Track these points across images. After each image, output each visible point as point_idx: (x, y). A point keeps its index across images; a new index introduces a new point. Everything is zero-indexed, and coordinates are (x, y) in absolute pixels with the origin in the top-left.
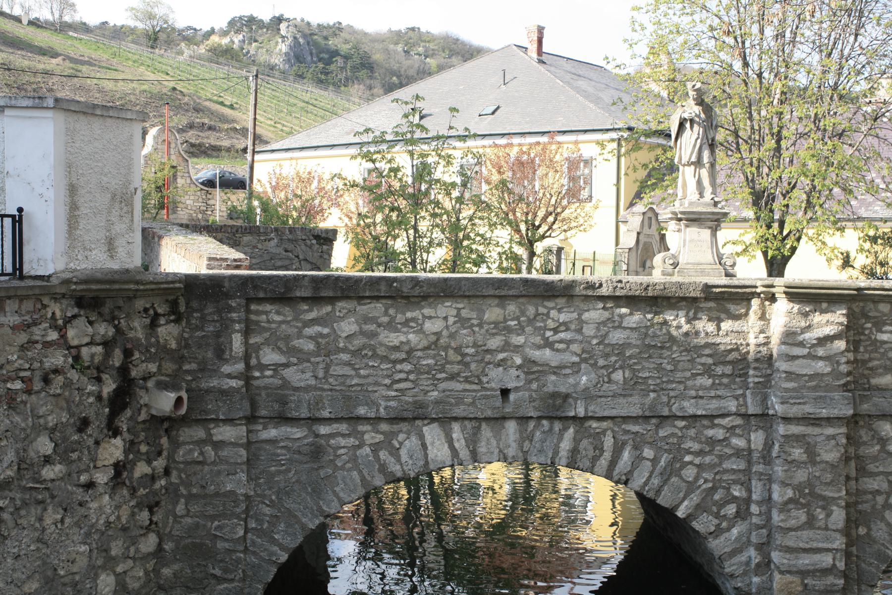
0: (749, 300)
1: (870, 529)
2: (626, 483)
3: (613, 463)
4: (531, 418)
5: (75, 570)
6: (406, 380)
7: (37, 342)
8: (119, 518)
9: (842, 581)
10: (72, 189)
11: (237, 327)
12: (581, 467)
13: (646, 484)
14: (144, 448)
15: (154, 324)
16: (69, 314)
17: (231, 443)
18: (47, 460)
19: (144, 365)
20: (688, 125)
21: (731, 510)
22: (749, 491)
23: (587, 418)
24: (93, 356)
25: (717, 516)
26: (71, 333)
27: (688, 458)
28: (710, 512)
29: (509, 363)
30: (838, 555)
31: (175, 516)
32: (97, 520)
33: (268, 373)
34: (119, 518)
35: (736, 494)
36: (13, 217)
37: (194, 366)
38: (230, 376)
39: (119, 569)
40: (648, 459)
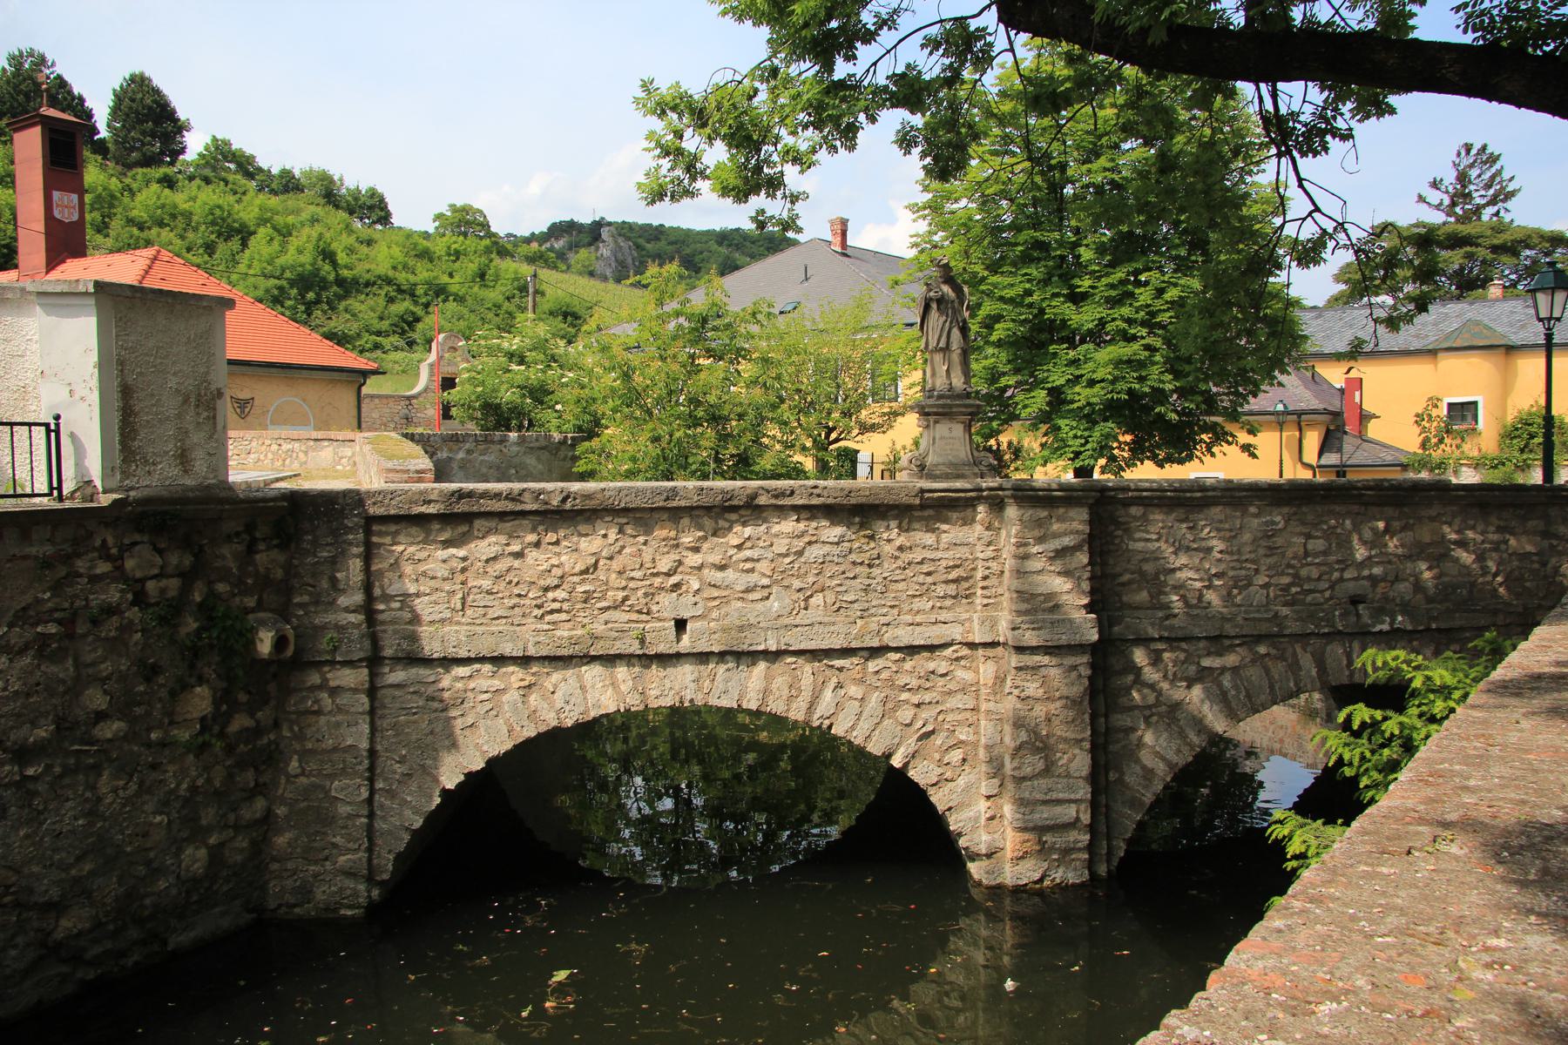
0: (974, 507)
1: (1122, 774)
5: (148, 845)
6: (559, 611)
7: (81, 576)
8: (209, 781)
9: (1088, 837)
10: (126, 392)
11: (355, 550)
13: (853, 728)
14: (243, 697)
15: (251, 550)
16: (127, 541)
17: (350, 689)
18: (100, 716)
19: (237, 599)
20: (934, 306)
21: (956, 756)
24: (163, 591)
26: (129, 564)
29: (684, 588)
30: (1083, 807)
31: (288, 776)
32: (178, 785)
33: (397, 605)
34: (209, 781)
36: (47, 425)
37: (306, 598)
38: (347, 610)
39: (212, 841)
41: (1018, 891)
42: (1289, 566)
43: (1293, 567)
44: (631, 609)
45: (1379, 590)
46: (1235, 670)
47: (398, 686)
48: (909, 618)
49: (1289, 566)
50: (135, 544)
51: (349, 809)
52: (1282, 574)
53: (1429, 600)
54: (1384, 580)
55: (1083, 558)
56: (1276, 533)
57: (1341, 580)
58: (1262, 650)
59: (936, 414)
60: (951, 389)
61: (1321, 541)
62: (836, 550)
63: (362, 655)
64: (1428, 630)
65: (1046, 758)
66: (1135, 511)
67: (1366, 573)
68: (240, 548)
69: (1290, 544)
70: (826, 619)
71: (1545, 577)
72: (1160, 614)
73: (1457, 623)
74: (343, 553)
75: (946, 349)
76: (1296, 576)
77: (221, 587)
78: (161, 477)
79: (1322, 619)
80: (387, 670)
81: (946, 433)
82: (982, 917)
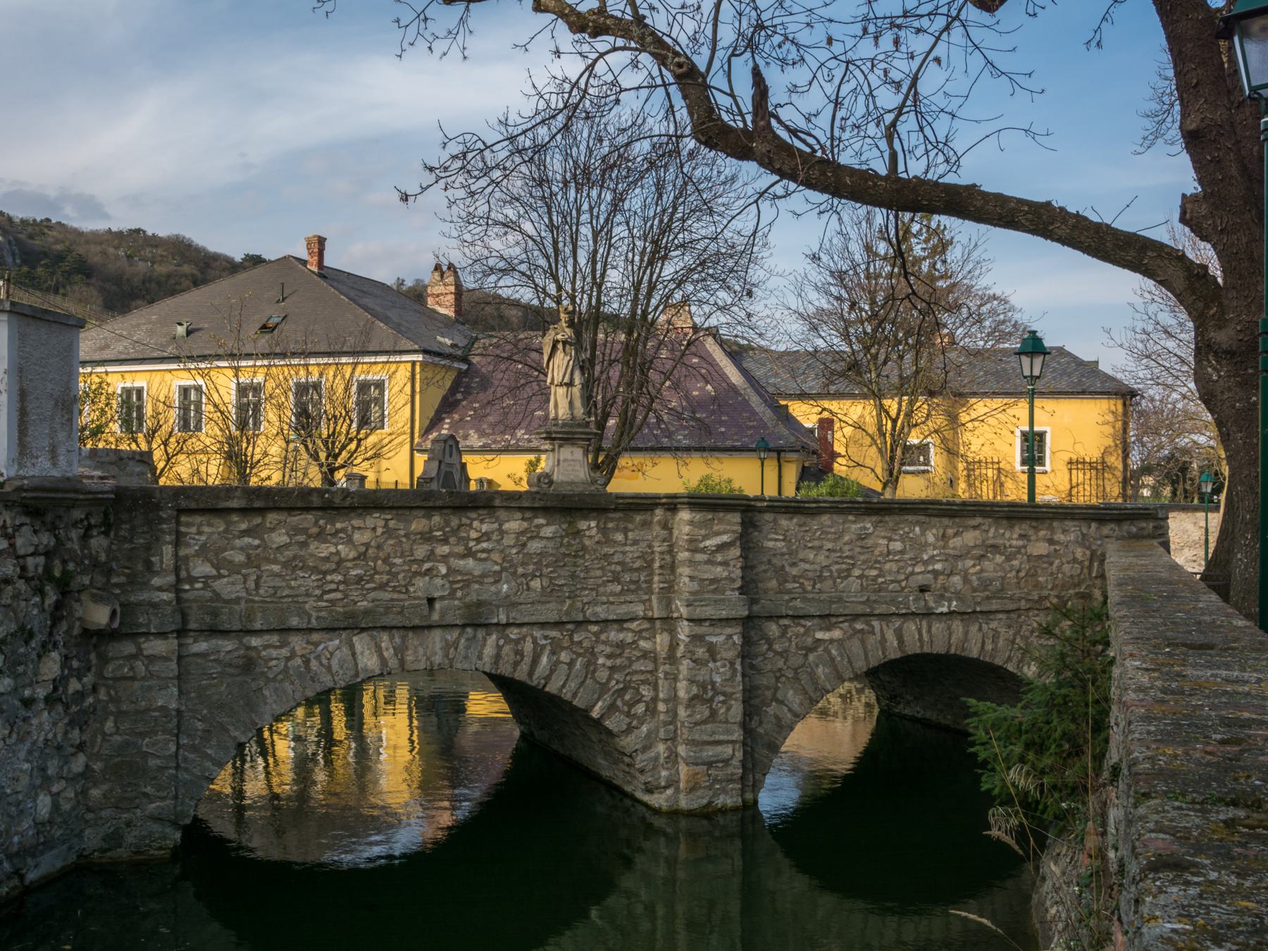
10: (23, 395)
11: (168, 538)
13: (563, 686)
16: (17, 523)
20: (560, 346)
26: (19, 542)
31: (104, 734)
33: (198, 585)
37: (123, 579)
38: (160, 589)
41: (690, 814)
42: (876, 562)
43: (879, 562)
44: (394, 589)
45: (940, 581)
46: (840, 642)
47: (202, 655)
49: (876, 562)
50: (22, 525)
51: (158, 762)
52: (871, 568)
53: (975, 590)
54: (942, 573)
55: (736, 552)
56: (868, 536)
57: (912, 573)
58: (859, 626)
59: (560, 439)
60: (573, 418)
61: (898, 543)
62: (550, 544)
63: (173, 627)
64: (974, 612)
66: (768, 517)
67: (930, 568)
69: (877, 545)
70: (543, 599)
71: (1052, 574)
72: (787, 597)
73: (994, 607)
74: (157, 539)
75: (570, 384)
76: (880, 570)
77: (71, 566)
78: (41, 468)
79: (900, 603)
80: (190, 641)
81: (569, 457)
82: (662, 839)
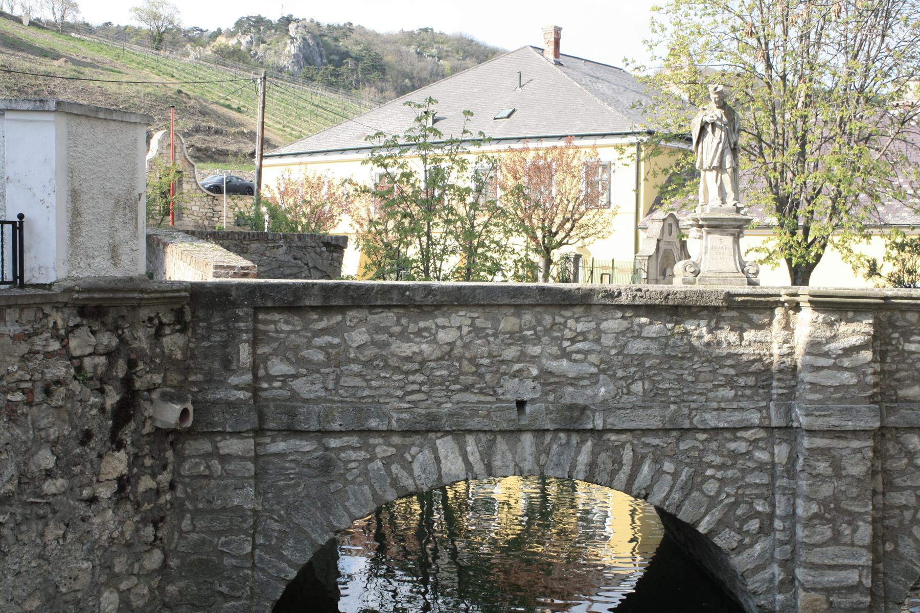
0: (773, 309)
1: (897, 545)
2: (645, 498)
3: (632, 477)
4: (548, 430)
5: (77, 588)
6: (419, 391)
7: (38, 352)
8: (122, 533)
9: (869, 599)
10: (75, 195)
11: (245, 336)
12: (599, 481)
13: (666, 498)
14: (148, 462)
15: (158, 334)
16: (71, 324)
17: (239, 456)
18: (49, 474)
20: (709, 129)
21: (754, 525)
22: (773, 506)
23: (605, 431)
24: (95, 367)
25: (739, 531)
26: (73, 343)
27: (709, 472)
28: (732, 528)
29: (525, 374)
30: (865, 572)
31: (181, 532)
33: (277, 384)
34: (122, 533)
35: (759, 508)
36: (13, 223)
37: (200, 377)
38: (237, 387)
39: (123, 586)
40: (668, 473)
48: (715, 405)
51: (234, 562)
65: (833, 529)
68: (152, 331)
